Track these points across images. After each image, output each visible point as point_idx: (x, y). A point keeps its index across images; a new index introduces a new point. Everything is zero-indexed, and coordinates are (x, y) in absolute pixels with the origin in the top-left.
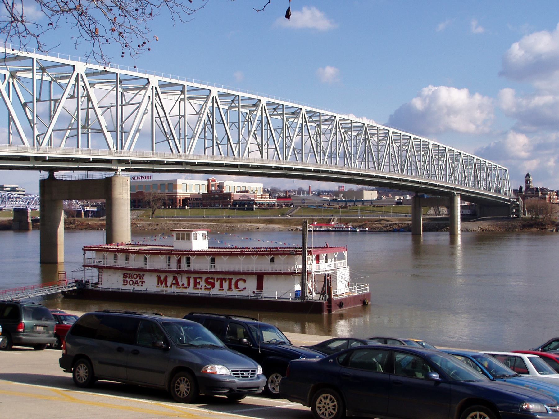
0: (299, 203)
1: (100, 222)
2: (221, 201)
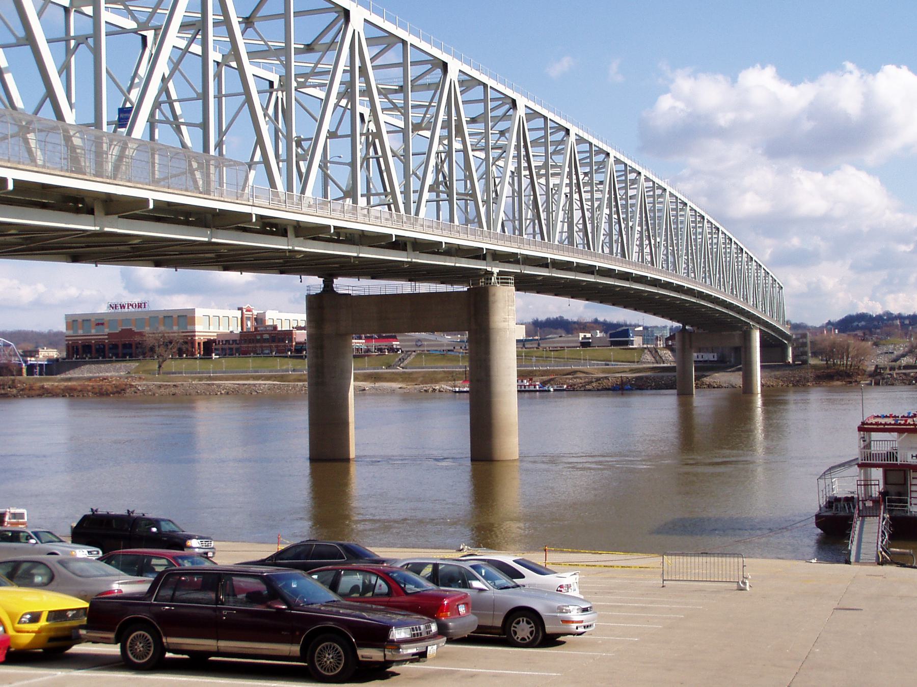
0: (412, 346)
1: (66, 384)
2: (273, 345)
